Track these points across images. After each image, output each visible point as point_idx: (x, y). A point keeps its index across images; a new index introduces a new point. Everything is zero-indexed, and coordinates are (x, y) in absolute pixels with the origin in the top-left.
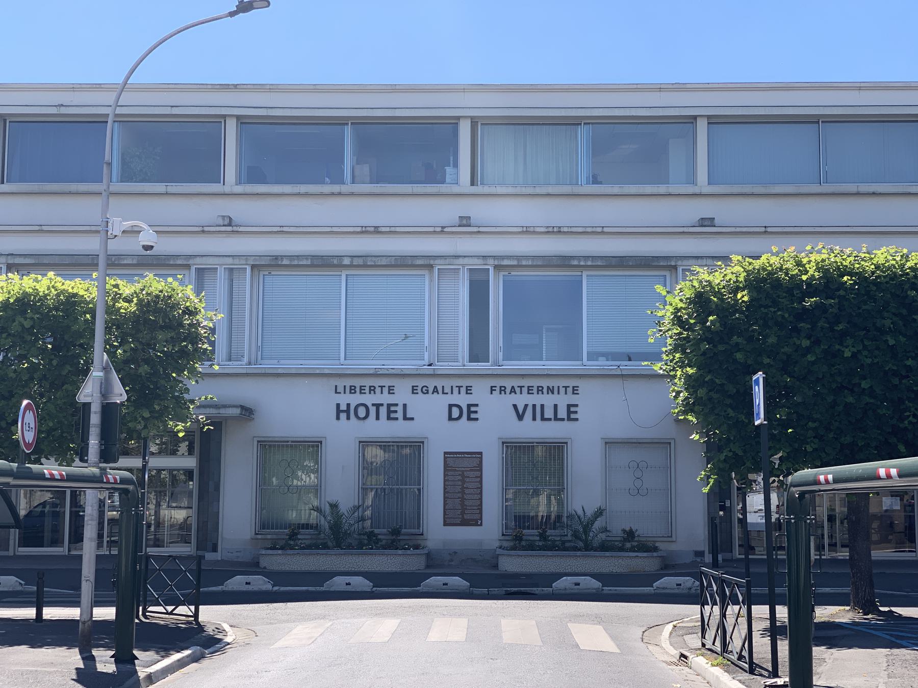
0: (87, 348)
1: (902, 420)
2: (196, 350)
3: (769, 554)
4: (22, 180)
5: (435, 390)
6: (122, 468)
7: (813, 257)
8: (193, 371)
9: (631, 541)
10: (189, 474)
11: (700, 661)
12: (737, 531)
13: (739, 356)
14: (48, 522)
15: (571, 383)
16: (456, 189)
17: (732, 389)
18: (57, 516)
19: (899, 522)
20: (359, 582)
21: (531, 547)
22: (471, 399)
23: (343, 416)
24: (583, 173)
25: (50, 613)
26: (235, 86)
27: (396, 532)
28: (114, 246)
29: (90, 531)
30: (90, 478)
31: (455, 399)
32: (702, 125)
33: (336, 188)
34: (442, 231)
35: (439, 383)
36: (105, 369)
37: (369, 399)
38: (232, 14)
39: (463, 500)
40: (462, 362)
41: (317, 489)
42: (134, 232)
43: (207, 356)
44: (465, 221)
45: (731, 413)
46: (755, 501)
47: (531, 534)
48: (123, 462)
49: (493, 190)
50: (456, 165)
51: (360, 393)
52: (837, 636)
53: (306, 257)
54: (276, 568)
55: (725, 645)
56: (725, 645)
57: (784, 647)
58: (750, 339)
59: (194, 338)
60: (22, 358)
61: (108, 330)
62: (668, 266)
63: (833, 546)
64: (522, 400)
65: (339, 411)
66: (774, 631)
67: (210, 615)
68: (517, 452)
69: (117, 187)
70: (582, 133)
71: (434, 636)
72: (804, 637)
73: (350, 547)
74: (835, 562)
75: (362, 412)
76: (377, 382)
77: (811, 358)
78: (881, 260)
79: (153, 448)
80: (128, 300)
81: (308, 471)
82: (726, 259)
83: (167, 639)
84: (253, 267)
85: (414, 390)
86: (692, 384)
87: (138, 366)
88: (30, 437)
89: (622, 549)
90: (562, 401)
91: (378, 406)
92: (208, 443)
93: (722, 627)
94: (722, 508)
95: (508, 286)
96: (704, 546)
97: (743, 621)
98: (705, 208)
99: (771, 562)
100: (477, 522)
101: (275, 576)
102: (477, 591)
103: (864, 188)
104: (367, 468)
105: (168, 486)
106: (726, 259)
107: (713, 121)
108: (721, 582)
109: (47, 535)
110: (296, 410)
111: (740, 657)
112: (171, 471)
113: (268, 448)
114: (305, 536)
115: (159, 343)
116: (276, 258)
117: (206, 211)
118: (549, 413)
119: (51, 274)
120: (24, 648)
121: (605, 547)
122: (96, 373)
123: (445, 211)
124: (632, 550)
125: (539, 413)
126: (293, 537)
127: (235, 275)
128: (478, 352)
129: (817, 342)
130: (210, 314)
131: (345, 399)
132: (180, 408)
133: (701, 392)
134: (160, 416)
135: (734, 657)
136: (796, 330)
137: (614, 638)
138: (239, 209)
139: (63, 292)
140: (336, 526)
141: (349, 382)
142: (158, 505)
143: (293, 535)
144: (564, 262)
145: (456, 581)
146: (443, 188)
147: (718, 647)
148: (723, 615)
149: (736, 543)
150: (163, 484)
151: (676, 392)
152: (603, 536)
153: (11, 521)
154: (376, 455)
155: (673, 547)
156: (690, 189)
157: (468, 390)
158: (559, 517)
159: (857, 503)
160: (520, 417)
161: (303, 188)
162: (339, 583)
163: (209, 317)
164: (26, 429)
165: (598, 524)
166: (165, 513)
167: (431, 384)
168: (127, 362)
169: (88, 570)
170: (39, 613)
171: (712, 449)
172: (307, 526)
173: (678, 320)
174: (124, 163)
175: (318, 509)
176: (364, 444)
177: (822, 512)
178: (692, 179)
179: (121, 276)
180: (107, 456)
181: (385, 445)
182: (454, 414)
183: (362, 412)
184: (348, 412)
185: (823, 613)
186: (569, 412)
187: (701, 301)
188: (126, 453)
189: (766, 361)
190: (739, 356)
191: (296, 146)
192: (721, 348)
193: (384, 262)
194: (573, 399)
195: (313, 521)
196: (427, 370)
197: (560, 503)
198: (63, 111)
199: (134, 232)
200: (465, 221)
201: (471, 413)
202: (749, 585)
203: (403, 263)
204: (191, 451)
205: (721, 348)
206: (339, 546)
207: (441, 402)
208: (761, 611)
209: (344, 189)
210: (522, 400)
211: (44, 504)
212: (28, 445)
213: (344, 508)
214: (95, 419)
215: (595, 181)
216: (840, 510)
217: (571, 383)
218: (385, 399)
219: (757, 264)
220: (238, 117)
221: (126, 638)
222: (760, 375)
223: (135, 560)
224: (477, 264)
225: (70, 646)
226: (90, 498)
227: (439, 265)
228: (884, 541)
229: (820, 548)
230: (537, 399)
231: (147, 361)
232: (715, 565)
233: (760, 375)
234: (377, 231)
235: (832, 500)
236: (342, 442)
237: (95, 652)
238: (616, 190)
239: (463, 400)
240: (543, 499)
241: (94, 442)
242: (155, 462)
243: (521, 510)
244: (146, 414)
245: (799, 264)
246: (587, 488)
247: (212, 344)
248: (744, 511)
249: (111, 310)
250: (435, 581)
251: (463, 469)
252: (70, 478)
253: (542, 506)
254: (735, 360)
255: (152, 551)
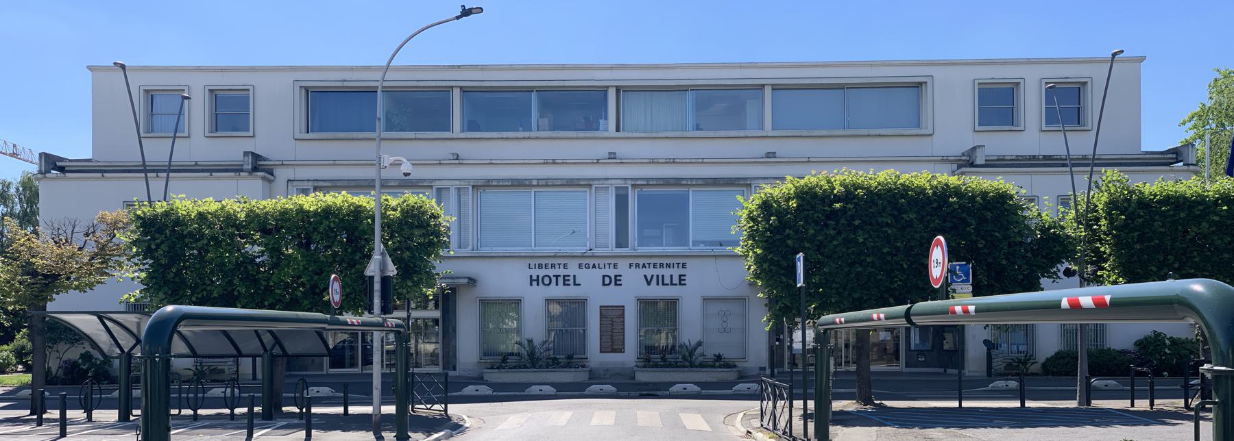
0: (370, 241)
1: (892, 283)
2: (439, 241)
3: (804, 368)
4: (321, 130)
5: (594, 266)
6: (396, 318)
7: (839, 177)
8: (437, 255)
9: (719, 361)
10: (436, 321)
11: (759, 435)
12: (787, 354)
13: (789, 242)
14: (348, 353)
15: (681, 261)
16: (606, 134)
17: (784, 264)
18: (353, 348)
19: (890, 348)
20: (548, 389)
21: (656, 366)
22: (616, 272)
23: (535, 283)
24: (690, 122)
25: (353, 410)
26: (459, 67)
27: (570, 357)
28: (385, 174)
29: (376, 358)
30: (375, 324)
31: (607, 272)
32: (768, 90)
33: (527, 134)
34: (598, 162)
35: (596, 262)
36: (382, 254)
37: (551, 272)
38: (458, 18)
39: (612, 336)
40: (612, 249)
41: (518, 331)
42: (398, 164)
43: (446, 245)
44: (612, 156)
45: (784, 279)
46: (798, 335)
47: (656, 357)
48: (396, 314)
49: (630, 135)
50: (606, 118)
51: (545, 269)
52: (846, 419)
53: (508, 180)
54: (494, 381)
55: (775, 425)
56: (775, 425)
57: (811, 426)
58: (797, 232)
59: (438, 234)
60: (327, 248)
61: (383, 228)
62: (745, 184)
63: (847, 363)
64: (650, 272)
65: (532, 280)
66: (806, 417)
67: (454, 410)
68: (646, 305)
69: (385, 135)
70: (689, 94)
71: (594, 422)
72: (824, 420)
73: (541, 367)
74: (848, 373)
75: (547, 281)
76: (556, 261)
77: (835, 243)
78: (882, 179)
79: (413, 306)
80: (395, 210)
81: (513, 319)
82: (783, 179)
83: (428, 425)
84: (473, 187)
85: (580, 266)
86: (759, 260)
87: (403, 252)
88: (337, 298)
89: (713, 367)
90: (676, 272)
91: (557, 277)
92: (447, 301)
93: (773, 414)
94: (778, 340)
95: (641, 198)
96: (766, 364)
97: (787, 410)
98: (770, 146)
99: (805, 373)
100: (621, 350)
101: (494, 386)
102: (621, 393)
103: (873, 132)
104: (550, 317)
105: (422, 329)
106: (783, 179)
107: (775, 88)
108: (774, 386)
109: (347, 361)
110: (504, 280)
111: (784, 433)
112: (424, 319)
113: (486, 304)
114: (512, 361)
115: (415, 237)
116: (488, 180)
117: (442, 150)
118: (667, 281)
119: (344, 192)
120: (338, 432)
121: (702, 366)
122: (376, 257)
123: (600, 149)
124: (720, 367)
125: (661, 281)
126: (504, 361)
127: (444, 192)
128: (621, 241)
129: (839, 233)
130: (447, 218)
131: (535, 273)
132: (430, 280)
133: (765, 266)
134: (417, 284)
135: (780, 433)
136: (826, 225)
137: (707, 422)
138: (463, 148)
139: (352, 204)
140: (532, 354)
141: (538, 262)
142: (417, 342)
143: (504, 360)
144: (677, 182)
145: (609, 388)
146: (597, 134)
147: (771, 427)
148: (775, 407)
149: (786, 361)
150: (418, 327)
151: (749, 266)
152: (701, 359)
153: (326, 352)
154: (556, 309)
155: (746, 365)
156: (760, 133)
157: (615, 266)
158: (673, 347)
159: (862, 335)
160: (649, 283)
161: (505, 134)
162: (535, 390)
163: (447, 220)
164: (335, 293)
165: (699, 351)
166: (421, 346)
167: (591, 262)
168: (395, 250)
169: (377, 382)
170: (346, 410)
171: (771, 302)
172: (512, 354)
173: (751, 218)
174: (388, 119)
175: (519, 343)
176: (549, 301)
177: (842, 343)
178: (762, 128)
179: (389, 194)
180: (385, 310)
181: (560, 302)
182: (606, 281)
183: (547, 281)
184: (537, 280)
185: (837, 405)
186: (680, 280)
187: (766, 206)
188: (396, 308)
189: (807, 245)
190: (789, 242)
191: (498, 105)
192: (778, 237)
193: (559, 182)
194: (682, 271)
195: (516, 351)
196: (589, 253)
197: (674, 338)
198: (346, 84)
199: (398, 164)
200: (612, 156)
201: (617, 280)
202: (791, 388)
203: (571, 183)
204: (436, 306)
205: (778, 237)
206: (534, 366)
207: (598, 273)
208: (798, 404)
209: (533, 134)
210: (650, 272)
211: (344, 341)
212: (336, 303)
213: (537, 342)
214: (377, 286)
215: (698, 129)
216: (852, 340)
217: (681, 261)
218: (562, 272)
219: (802, 182)
220: (461, 88)
221: (403, 424)
222: (801, 255)
223: (407, 375)
224: (620, 183)
225: (368, 430)
226: (377, 336)
227: (596, 184)
228: (880, 359)
229: (838, 364)
230: (660, 271)
231: (408, 249)
232: (772, 376)
233: (801, 255)
234: (554, 162)
235: (848, 334)
236: (535, 300)
237: (383, 434)
238: (711, 134)
239: (612, 273)
240: (663, 335)
241: (377, 301)
242: (415, 314)
243: (649, 343)
244: (410, 284)
245: (829, 182)
246: (690, 330)
247: (449, 237)
248: (792, 341)
249: (384, 216)
250: (595, 388)
251: (612, 317)
252: (364, 324)
253: (663, 340)
254: (787, 246)
255: (416, 370)
